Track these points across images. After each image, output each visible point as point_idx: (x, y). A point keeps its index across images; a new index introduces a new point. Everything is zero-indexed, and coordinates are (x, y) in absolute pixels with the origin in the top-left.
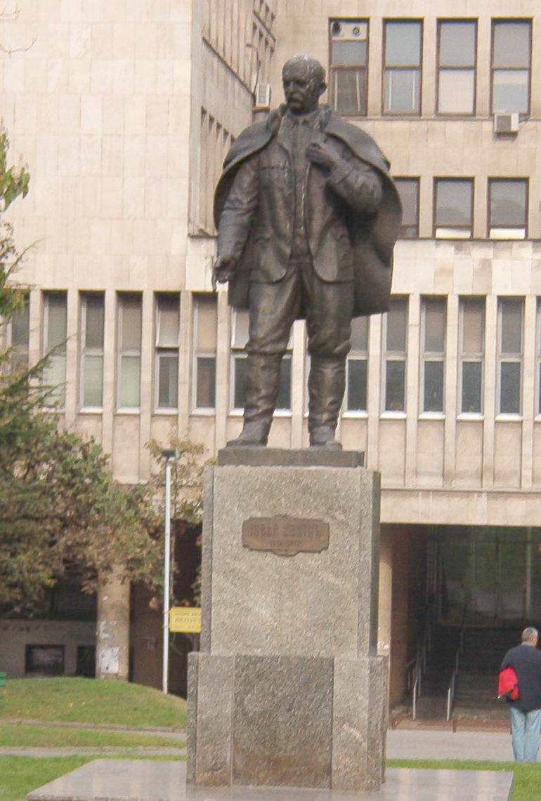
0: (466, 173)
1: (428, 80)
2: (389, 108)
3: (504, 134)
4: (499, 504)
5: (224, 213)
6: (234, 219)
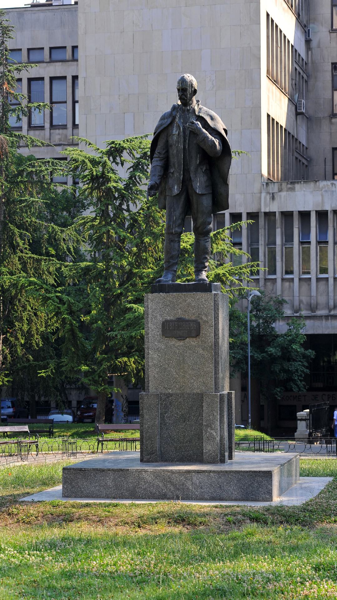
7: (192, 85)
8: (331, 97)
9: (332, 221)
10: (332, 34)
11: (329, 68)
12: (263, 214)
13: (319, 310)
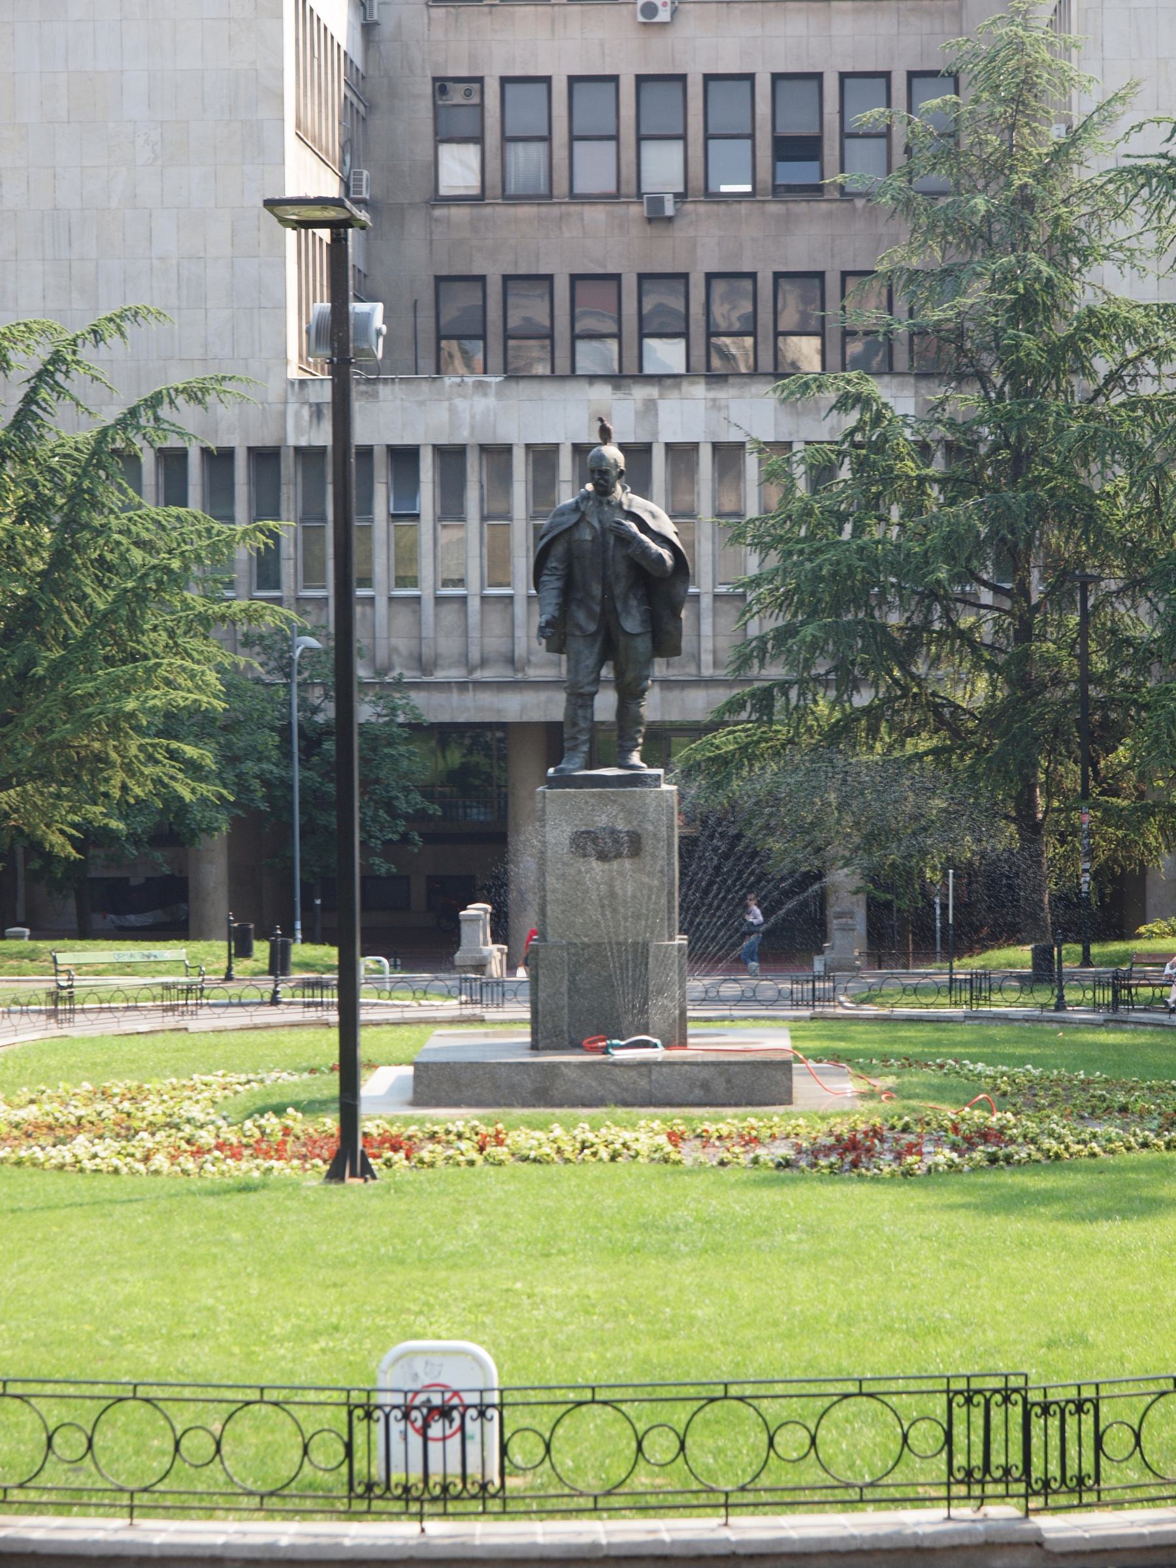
0: (611, 269)
1: (560, 153)
2: (512, 189)
3: (656, 218)
4: (675, 695)
5: (544, 578)
6: (553, 584)
7: (617, 466)
8: (431, 158)
9: (476, 468)
10: (432, 10)
11: (428, 89)
12: (292, 452)
13: (443, 669)
